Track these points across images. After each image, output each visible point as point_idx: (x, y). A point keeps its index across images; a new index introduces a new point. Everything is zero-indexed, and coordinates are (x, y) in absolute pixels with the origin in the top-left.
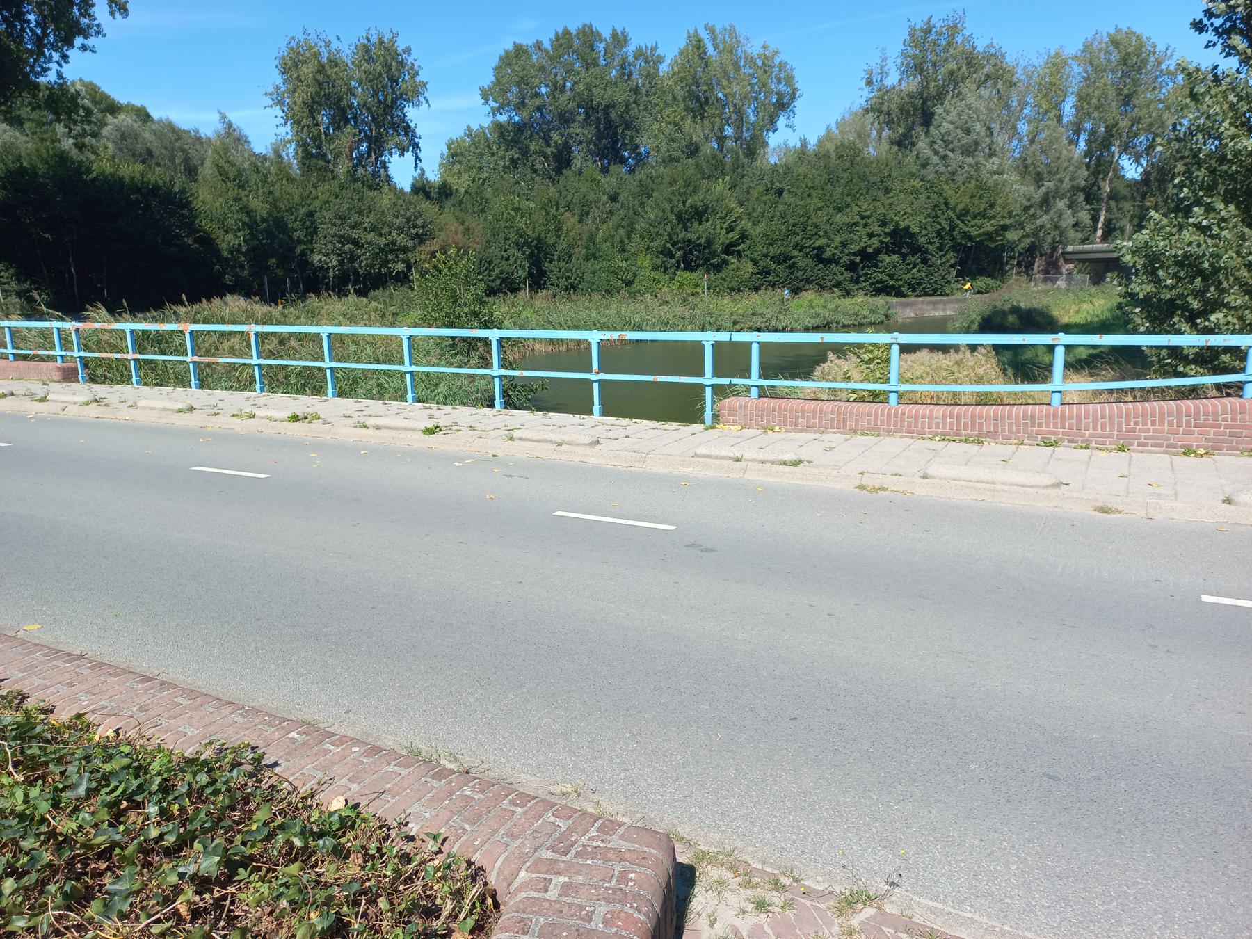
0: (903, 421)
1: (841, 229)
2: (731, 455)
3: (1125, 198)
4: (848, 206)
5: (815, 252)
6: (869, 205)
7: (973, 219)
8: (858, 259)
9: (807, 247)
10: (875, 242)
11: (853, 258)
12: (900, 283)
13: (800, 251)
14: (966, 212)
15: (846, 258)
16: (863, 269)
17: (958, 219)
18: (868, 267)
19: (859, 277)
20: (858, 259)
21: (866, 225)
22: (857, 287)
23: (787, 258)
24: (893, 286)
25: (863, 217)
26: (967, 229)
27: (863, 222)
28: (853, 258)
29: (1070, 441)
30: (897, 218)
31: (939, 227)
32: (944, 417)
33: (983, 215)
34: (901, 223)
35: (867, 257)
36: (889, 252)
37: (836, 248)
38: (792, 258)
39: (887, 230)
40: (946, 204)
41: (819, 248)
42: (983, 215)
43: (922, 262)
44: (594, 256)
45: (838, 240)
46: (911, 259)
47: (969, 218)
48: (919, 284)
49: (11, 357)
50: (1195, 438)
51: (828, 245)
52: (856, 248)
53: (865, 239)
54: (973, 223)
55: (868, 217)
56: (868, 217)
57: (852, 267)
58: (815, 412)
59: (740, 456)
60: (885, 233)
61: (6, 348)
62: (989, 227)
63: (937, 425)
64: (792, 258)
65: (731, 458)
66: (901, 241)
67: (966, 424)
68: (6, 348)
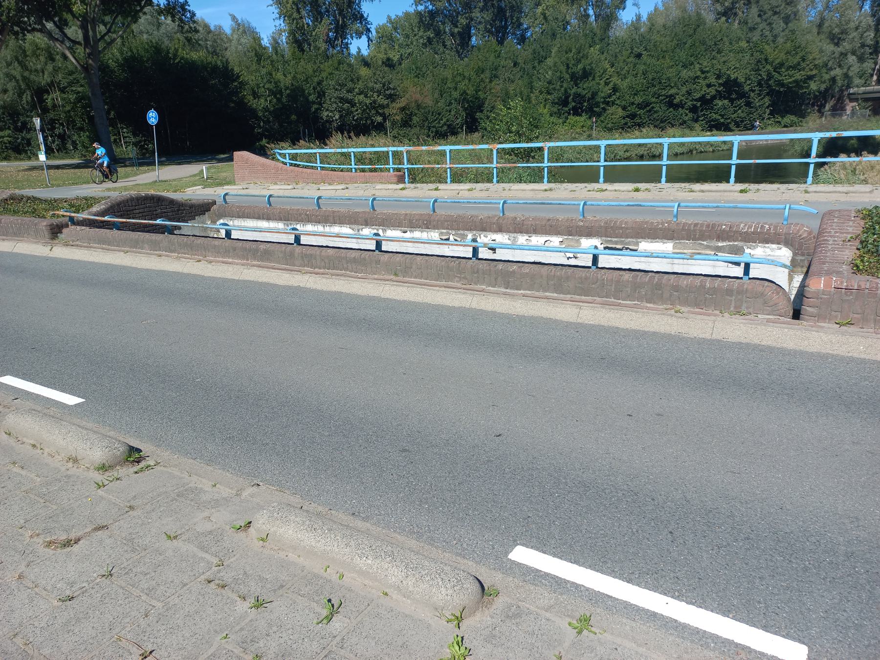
1: (687, 81)
6: (708, 62)
8: (699, 104)
9: (661, 96)
10: (712, 91)
12: (729, 121)
15: (690, 103)
16: (702, 111)
17: (774, 71)
20: (699, 104)
21: (705, 78)
23: (648, 104)
27: (703, 76)
28: (695, 103)
30: (728, 72)
31: (759, 78)
33: (794, 67)
34: (732, 76)
35: (706, 102)
37: (683, 96)
38: (651, 104)
39: (720, 81)
45: (684, 89)
48: (742, 121)
52: (697, 95)
53: (705, 88)
54: (786, 73)
55: (708, 72)
56: (708, 72)
57: (694, 109)
61: (404, 164)
62: (798, 76)
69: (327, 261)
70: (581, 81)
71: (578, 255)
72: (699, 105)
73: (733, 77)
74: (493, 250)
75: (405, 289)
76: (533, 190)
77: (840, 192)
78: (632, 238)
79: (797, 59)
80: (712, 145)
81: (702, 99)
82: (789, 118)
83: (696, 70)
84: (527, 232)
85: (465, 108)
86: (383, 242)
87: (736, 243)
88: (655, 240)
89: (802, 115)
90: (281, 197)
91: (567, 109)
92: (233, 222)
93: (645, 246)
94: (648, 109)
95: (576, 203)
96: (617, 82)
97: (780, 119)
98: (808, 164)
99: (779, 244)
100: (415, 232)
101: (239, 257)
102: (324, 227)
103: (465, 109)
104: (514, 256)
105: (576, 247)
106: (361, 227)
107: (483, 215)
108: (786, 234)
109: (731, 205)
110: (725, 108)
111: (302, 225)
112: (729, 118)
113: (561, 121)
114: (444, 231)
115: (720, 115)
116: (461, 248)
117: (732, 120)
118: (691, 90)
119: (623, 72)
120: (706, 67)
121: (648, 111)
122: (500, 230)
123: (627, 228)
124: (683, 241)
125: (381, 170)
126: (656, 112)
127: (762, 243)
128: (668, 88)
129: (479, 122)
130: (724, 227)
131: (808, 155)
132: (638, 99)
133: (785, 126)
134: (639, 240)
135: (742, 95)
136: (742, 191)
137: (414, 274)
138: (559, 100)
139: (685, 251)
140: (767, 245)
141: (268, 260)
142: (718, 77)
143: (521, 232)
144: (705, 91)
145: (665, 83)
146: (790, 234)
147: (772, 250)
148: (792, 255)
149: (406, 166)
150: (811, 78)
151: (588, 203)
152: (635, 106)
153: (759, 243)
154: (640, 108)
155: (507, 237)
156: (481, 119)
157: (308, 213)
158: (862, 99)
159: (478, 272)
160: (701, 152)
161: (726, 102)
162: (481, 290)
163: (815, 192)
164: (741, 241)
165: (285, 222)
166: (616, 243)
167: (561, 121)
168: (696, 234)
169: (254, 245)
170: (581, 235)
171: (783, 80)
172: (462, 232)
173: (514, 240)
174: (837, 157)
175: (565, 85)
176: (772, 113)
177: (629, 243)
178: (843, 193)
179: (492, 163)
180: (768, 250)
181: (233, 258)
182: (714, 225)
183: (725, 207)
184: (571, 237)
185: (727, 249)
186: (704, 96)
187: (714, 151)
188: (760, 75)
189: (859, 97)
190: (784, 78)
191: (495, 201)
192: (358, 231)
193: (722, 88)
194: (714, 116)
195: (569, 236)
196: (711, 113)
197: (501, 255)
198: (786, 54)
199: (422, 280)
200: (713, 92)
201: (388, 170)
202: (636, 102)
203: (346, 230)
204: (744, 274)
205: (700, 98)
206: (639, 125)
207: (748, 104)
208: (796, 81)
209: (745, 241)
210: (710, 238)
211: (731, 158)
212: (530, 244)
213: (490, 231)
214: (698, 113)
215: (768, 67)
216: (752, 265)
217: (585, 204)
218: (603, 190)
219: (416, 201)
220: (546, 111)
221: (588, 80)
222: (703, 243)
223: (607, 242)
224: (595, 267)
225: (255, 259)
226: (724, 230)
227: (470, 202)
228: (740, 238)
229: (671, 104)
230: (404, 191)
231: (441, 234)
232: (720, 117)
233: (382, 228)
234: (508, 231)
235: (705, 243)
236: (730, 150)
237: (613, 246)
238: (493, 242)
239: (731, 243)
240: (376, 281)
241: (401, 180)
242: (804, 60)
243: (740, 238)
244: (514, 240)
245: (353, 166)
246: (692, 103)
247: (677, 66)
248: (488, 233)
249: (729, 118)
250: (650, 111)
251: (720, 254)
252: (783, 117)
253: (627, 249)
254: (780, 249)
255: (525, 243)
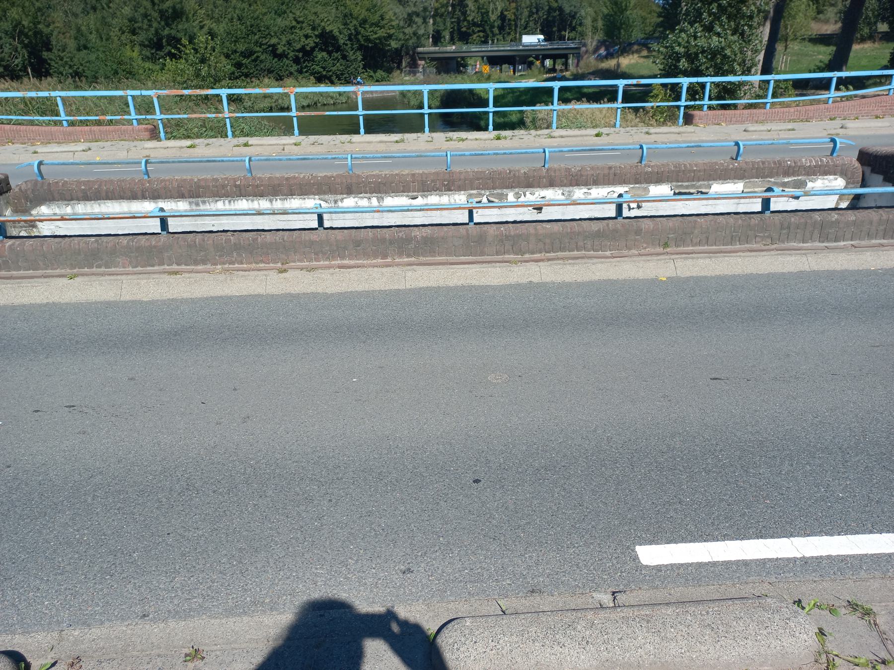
0: (778, 115)
1: (284, 30)
2: (766, 129)
3: (34, 7)
4: (285, 12)
5: (271, 49)
6: (301, 12)
7: (370, 27)
8: (301, 55)
9: (264, 44)
10: (310, 43)
11: (297, 54)
12: (331, 73)
13: (260, 47)
14: (365, 21)
15: (292, 54)
16: (304, 62)
17: (360, 26)
18: (308, 61)
19: (302, 68)
20: (301, 55)
21: (301, 28)
22: (301, 76)
23: (252, 53)
24: (326, 75)
25: (298, 22)
26: (367, 34)
27: (299, 26)
28: (297, 54)
29: (862, 116)
30: (323, 24)
31: (349, 32)
32: (794, 111)
33: (376, 25)
34: (327, 28)
35: (309, 52)
36: (321, 50)
37: (284, 46)
38: (255, 52)
39: (316, 33)
40: (351, 15)
41: (274, 46)
42: (376, 25)
43: (342, 58)
44: (86, 47)
45: (284, 40)
46: (336, 55)
47: (367, 26)
48: (342, 74)
49: (65, 123)
50: (879, 113)
51: (279, 44)
52: (298, 46)
53: (303, 39)
54: (371, 29)
55: (303, 22)
56: (303, 22)
57: (296, 61)
58: (740, 115)
59: (769, 129)
60: (316, 36)
61: (130, 115)
62: (381, 33)
63: (791, 116)
64: (255, 52)
65: (765, 131)
66: (327, 41)
67: (803, 114)
68: (130, 115)
69: (548, 241)
70: (173, 22)
71: (644, 204)
72: (301, 56)
73: (328, 29)
74: (539, 209)
75: (708, 261)
76: (381, 142)
77: (673, 133)
78: (703, 180)
79: (376, 17)
80: (332, 98)
81: (302, 49)
82: (380, 73)
83: (288, 22)
84: (586, 184)
85: (24, 44)
86: (169, 219)
87: (800, 178)
88: (727, 181)
89: (389, 71)
90: (78, 164)
91: (162, 54)
92: (73, 208)
93: (717, 188)
94: (253, 57)
95: (344, 156)
96: (211, 26)
97: (372, 74)
98: (678, 107)
99: (835, 174)
100: (429, 197)
101: (366, 255)
102: (271, 201)
103: (26, 46)
104: (563, 214)
105: (643, 195)
106: (339, 197)
107: (523, 168)
108: (842, 164)
109: (785, 141)
110: (325, 61)
111: (227, 202)
112: (330, 71)
113: (158, 67)
114: (474, 192)
115: (322, 67)
116: (496, 211)
117: (333, 73)
118: (290, 40)
119: (216, 16)
120: (300, 17)
121: (253, 61)
122: (551, 184)
123: (699, 171)
124: (752, 180)
125: (117, 122)
126: (261, 61)
127: (823, 175)
128: (269, 36)
129: (49, 65)
130: (789, 163)
131: (422, 107)
132: (241, 47)
133: (377, 81)
134: (710, 182)
135: (338, 49)
136: (597, 135)
137: (695, 241)
138: (150, 42)
139: (756, 190)
140: (826, 177)
141: (432, 253)
142: (314, 29)
143: (578, 185)
144: (304, 42)
145: (264, 31)
146: (846, 164)
147: (830, 181)
148: (845, 184)
149: (158, 116)
150: (390, 36)
151: (253, 159)
152: (238, 54)
153: (819, 175)
154: (245, 57)
155: (560, 192)
156: (51, 60)
157: (238, 183)
158: (428, 58)
159: (789, 228)
160: (325, 105)
161: (324, 54)
162: (191, 270)
163: (656, 133)
164: (804, 175)
165: (191, 200)
166: (687, 187)
167: (158, 67)
168: (765, 172)
169: (402, 233)
170: (650, 181)
171: (369, 36)
172: (499, 191)
173: (569, 195)
174: (534, 106)
175: (155, 25)
176: (364, 67)
177: (700, 187)
178: (676, 133)
179: (154, 113)
180: (826, 181)
181: (357, 257)
182: (780, 162)
183: (779, 144)
184: (637, 185)
185: (792, 184)
186: (303, 47)
187: (334, 104)
188: (350, 29)
189: (426, 56)
190: (370, 34)
191: (531, 150)
192: (336, 202)
193: (318, 40)
194: (317, 67)
195: (636, 184)
196: (313, 65)
197: (549, 213)
198: (367, 10)
199: (22, 272)
200: (312, 45)
201: (130, 122)
202: (238, 50)
203: (402, 201)
204: (319, 226)
205: (300, 49)
206: (246, 76)
207: (344, 57)
208: (379, 38)
209: (808, 175)
210: (778, 174)
211: (357, 109)
212: (589, 197)
213: (539, 187)
214: (300, 64)
215: (355, 22)
216: (475, 211)
217: (250, 160)
218: (463, 140)
219: (418, 156)
220: (135, 54)
221: (182, 21)
222: (770, 180)
223: (677, 187)
224: (165, 232)
225: (400, 255)
226: (790, 167)
227: (366, 158)
228: (803, 172)
229: (275, 54)
230: (191, 150)
231: (470, 196)
232: (322, 70)
233: (376, 195)
234: (561, 185)
235: (773, 180)
236: (616, 92)
237: (687, 191)
238: (541, 200)
239: (796, 178)
240: (644, 258)
241: (154, 135)
242: (383, 19)
243: (803, 172)
244: (569, 195)
245: (63, 116)
246: (293, 53)
247: (270, 13)
248: (535, 190)
249: (330, 71)
250: (255, 60)
251: (786, 190)
252: (375, 72)
253: (698, 192)
254: (836, 179)
255: (582, 197)
